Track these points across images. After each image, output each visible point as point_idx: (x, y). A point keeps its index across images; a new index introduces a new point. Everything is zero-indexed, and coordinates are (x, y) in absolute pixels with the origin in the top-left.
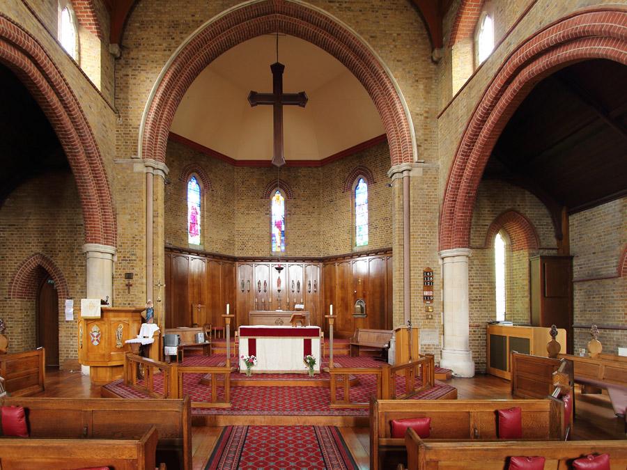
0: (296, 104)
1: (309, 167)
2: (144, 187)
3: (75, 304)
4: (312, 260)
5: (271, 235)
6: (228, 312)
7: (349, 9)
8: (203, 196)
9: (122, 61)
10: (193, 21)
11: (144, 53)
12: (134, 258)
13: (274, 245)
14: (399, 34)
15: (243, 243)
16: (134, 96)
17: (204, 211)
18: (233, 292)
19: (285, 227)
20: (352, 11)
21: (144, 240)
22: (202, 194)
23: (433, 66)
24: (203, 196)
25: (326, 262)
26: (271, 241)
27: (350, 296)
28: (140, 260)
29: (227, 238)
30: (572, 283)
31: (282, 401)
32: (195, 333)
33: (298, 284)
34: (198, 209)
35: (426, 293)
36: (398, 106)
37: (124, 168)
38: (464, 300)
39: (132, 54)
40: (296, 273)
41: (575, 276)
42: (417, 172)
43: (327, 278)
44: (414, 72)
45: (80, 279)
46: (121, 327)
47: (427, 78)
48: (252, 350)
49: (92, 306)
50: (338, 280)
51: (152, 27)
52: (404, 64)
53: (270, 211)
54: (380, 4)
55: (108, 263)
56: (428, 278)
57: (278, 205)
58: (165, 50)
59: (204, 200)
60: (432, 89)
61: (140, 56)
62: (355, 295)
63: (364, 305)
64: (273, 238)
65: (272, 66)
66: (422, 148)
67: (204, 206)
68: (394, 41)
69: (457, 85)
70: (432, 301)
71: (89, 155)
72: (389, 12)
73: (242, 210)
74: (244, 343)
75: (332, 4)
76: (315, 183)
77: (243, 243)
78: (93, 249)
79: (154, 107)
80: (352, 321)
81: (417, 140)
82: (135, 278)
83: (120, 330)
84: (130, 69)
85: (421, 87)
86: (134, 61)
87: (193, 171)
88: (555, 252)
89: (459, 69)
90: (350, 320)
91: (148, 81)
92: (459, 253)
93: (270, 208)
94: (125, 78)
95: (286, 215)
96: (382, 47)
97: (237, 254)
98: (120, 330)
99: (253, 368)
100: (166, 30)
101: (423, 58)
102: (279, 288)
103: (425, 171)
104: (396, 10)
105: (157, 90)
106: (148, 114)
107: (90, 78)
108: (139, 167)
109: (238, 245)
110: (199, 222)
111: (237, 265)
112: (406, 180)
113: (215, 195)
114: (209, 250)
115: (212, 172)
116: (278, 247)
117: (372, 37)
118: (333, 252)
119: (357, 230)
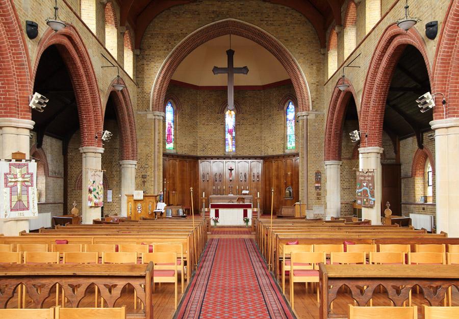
0: (241, 73)
1: (254, 90)
2: (153, 127)
3: (112, 192)
4: (256, 158)
5: (225, 140)
6: (204, 196)
7: (272, 24)
8: (176, 115)
9: (141, 57)
10: (182, 33)
11: (153, 52)
12: (147, 166)
13: (227, 147)
14: (301, 38)
15: (204, 146)
16: (148, 76)
17: (176, 125)
18: (196, 182)
19: (236, 134)
20: (274, 25)
21: (153, 157)
22: (175, 113)
23: (321, 56)
24: (176, 115)
25: (266, 159)
26: (225, 144)
27: (283, 186)
28: (151, 168)
29: (192, 143)
30: (401, 179)
31: (237, 310)
32: (177, 209)
33: (245, 176)
34: (172, 124)
35: (317, 185)
36: (301, 79)
37: (141, 117)
38: (335, 189)
39: (147, 52)
40: (242, 166)
41: (402, 175)
42: (312, 116)
43: (266, 171)
44: (311, 60)
45: (116, 179)
46: (151, 204)
47: (318, 63)
48: (217, 215)
49: (138, 194)
50: (274, 173)
51: (158, 37)
52: (305, 55)
53: (225, 123)
54: (291, 21)
55: (134, 171)
56: (319, 177)
57: (230, 119)
58: (165, 50)
59: (176, 117)
60: (321, 69)
61: (151, 54)
62: (286, 184)
63: (291, 191)
64: (227, 142)
65: (227, 52)
66: (315, 103)
67: (176, 122)
68: (299, 42)
69: (330, 75)
70: (320, 189)
71: (129, 116)
72: (296, 25)
73: (203, 122)
74: (213, 211)
75: (262, 22)
76: (258, 102)
77: (204, 146)
78: (128, 163)
79: (159, 81)
80: (284, 202)
81: (312, 98)
82: (148, 177)
83: (150, 205)
84: (145, 61)
85: (315, 68)
86: (147, 56)
87: (169, 99)
88: (394, 161)
89: (332, 64)
90: (282, 201)
91: (156, 67)
92: (333, 163)
93: (224, 120)
94: (142, 66)
95: (236, 125)
96: (292, 46)
97: (199, 154)
98: (150, 205)
99: (218, 224)
100: (166, 39)
101: (316, 52)
102: (231, 179)
103: (317, 116)
104: (300, 24)
105: (161, 73)
106: (155, 86)
107: (128, 73)
108: (150, 116)
109: (200, 147)
110: (173, 134)
111: (199, 162)
112: (305, 121)
113: (184, 113)
114: (180, 152)
115: (182, 97)
116: (230, 148)
117: (285, 40)
118: (270, 152)
119: (288, 138)
